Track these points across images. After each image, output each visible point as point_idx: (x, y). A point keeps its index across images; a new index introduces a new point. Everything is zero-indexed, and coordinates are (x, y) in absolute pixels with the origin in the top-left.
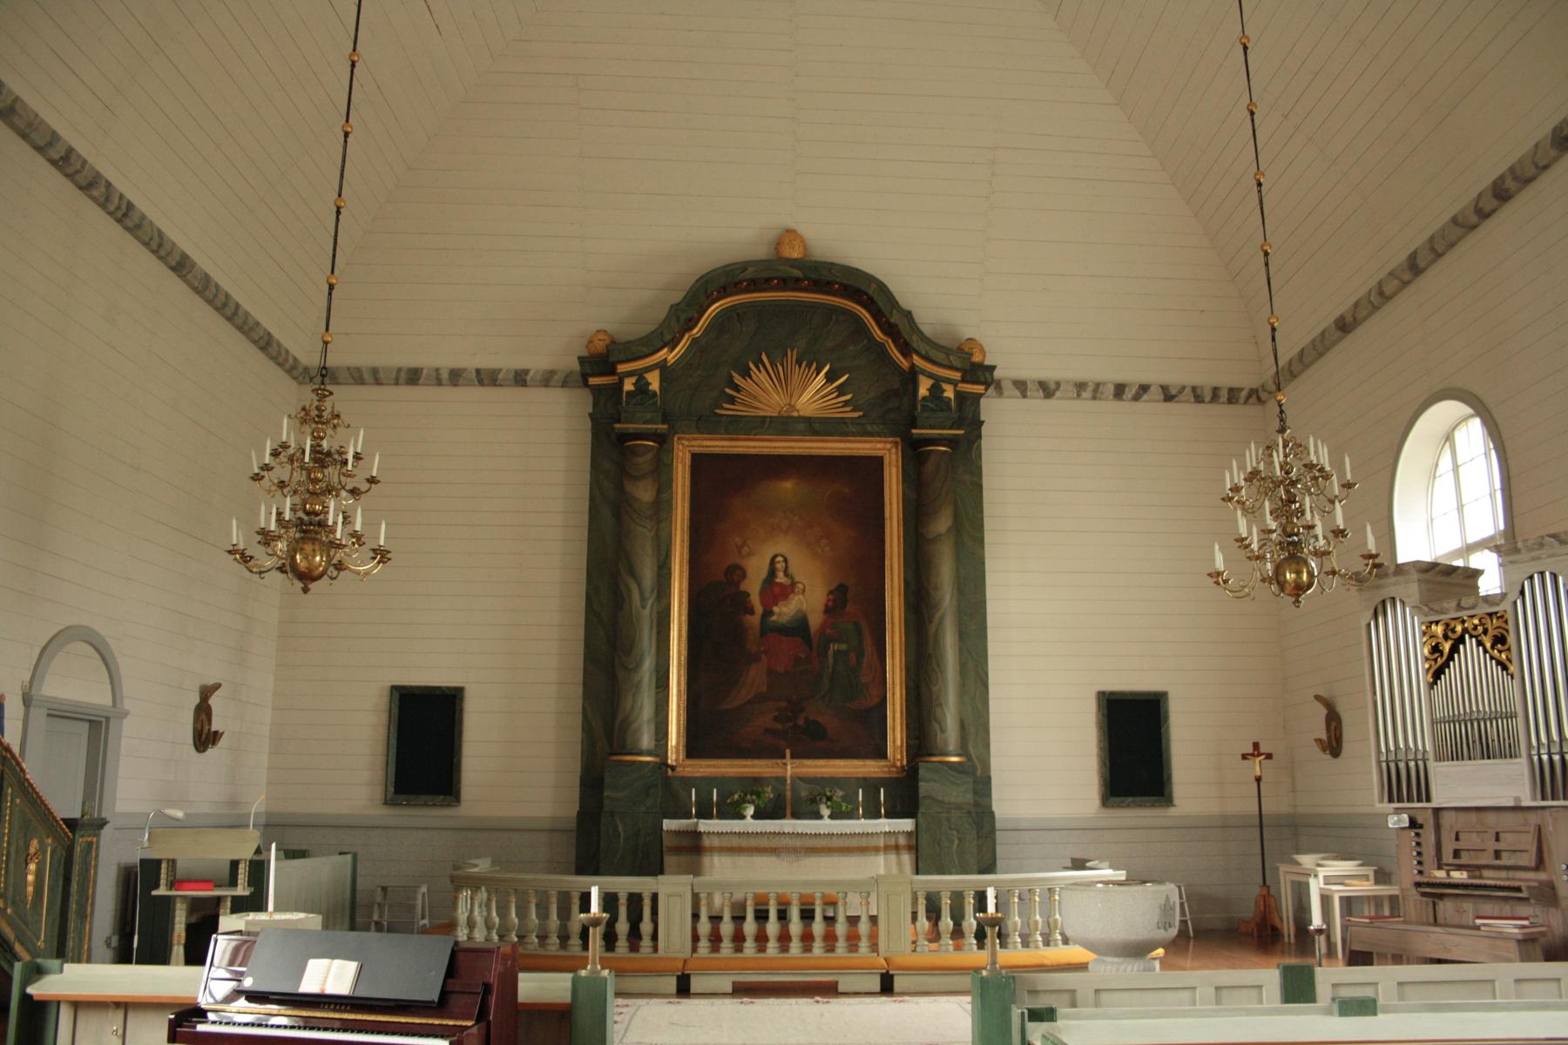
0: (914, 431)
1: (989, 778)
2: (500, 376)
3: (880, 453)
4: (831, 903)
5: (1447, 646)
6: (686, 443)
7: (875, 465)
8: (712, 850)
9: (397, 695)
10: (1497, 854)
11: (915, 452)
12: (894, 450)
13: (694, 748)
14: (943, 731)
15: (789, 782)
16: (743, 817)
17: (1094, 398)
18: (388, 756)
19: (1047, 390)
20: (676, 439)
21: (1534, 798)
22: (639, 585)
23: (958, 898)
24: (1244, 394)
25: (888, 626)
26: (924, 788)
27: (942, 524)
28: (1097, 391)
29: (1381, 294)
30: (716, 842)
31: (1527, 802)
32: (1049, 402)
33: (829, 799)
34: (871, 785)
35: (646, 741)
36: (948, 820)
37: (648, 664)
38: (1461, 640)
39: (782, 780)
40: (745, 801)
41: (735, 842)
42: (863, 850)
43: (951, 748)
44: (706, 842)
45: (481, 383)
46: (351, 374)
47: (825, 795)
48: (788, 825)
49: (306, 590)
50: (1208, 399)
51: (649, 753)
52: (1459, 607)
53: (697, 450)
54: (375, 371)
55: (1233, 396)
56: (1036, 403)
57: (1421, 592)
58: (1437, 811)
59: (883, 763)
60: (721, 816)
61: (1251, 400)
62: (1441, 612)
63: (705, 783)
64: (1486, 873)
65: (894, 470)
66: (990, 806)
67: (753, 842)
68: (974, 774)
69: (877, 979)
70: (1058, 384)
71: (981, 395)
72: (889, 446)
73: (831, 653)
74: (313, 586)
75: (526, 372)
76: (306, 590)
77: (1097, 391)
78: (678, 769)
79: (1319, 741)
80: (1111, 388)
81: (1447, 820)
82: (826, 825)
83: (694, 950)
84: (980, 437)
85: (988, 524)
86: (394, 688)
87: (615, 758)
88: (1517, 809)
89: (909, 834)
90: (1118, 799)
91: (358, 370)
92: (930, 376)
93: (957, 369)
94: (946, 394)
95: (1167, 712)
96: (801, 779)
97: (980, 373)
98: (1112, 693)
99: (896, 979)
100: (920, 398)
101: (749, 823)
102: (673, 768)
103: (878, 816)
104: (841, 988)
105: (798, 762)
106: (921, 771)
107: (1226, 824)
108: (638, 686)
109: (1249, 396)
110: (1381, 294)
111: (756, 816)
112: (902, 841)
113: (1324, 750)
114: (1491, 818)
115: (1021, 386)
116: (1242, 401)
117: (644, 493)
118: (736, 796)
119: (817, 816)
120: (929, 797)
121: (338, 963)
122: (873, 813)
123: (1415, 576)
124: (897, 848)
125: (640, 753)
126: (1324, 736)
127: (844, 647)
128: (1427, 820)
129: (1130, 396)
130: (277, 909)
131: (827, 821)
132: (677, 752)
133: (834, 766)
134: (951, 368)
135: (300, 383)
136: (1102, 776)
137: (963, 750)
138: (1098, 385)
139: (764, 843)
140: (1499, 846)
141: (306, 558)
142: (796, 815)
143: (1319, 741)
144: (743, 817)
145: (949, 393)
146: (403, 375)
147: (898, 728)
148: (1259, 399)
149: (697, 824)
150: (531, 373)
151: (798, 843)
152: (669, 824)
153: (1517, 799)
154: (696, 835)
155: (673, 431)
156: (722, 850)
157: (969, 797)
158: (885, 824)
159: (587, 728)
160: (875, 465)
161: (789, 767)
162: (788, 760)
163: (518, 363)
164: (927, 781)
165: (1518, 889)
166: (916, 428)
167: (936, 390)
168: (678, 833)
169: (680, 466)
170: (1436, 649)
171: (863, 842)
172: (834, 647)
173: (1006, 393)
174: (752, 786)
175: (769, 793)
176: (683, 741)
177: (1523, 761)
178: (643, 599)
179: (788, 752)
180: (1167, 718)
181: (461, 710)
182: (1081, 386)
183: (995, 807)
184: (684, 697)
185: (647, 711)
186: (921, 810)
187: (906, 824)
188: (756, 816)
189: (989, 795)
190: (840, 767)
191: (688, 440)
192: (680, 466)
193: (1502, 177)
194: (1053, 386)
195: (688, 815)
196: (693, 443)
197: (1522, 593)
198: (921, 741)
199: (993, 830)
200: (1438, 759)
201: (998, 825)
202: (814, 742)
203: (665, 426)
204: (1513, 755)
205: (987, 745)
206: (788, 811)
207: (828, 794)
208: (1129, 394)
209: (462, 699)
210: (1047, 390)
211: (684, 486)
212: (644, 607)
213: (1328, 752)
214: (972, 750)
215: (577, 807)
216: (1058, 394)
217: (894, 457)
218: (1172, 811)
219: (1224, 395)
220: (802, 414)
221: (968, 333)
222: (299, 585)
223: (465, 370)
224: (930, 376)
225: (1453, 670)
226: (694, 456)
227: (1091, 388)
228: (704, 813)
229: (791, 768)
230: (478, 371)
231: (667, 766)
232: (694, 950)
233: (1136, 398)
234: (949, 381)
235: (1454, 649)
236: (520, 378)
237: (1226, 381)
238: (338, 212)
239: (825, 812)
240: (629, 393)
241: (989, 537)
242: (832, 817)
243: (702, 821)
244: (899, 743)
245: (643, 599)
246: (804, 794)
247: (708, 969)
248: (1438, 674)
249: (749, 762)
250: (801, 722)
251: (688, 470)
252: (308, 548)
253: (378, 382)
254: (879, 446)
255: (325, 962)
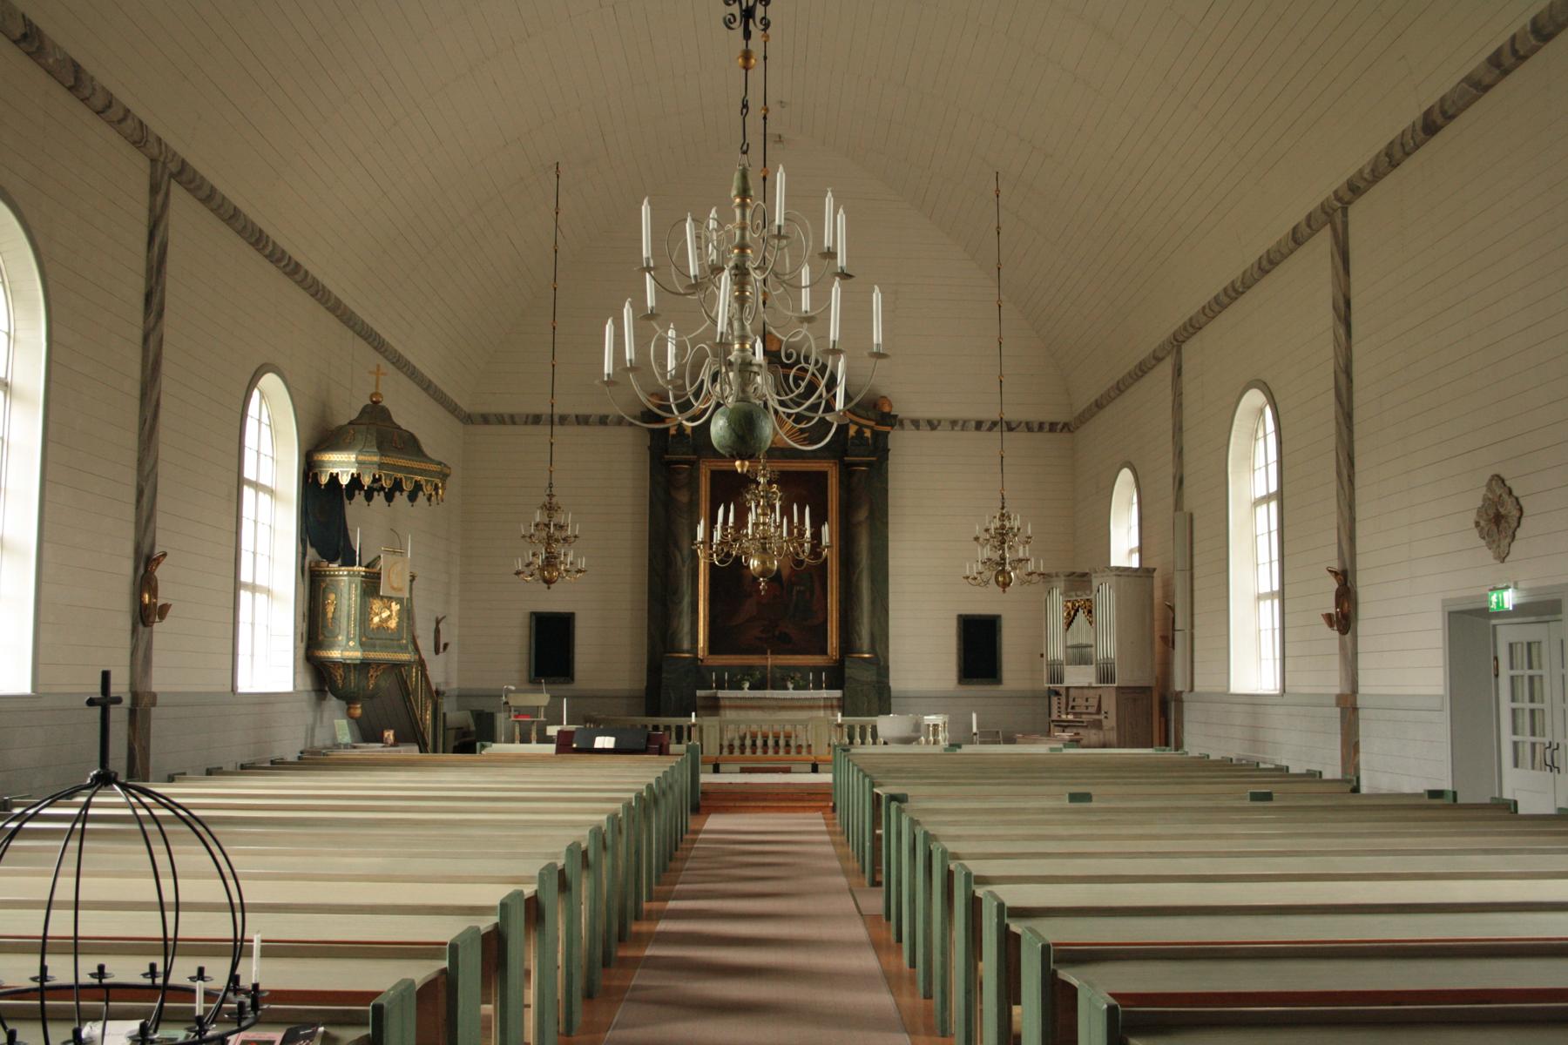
0: (846, 458)
1: (888, 667)
2: (591, 420)
3: (826, 469)
4: (788, 737)
5: (1072, 613)
6: (707, 464)
7: (823, 476)
8: (725, 707)
9: (534, 617)
10: (1087, 707)
11: (847, 471)
12: (834, 468)
13: (713, 648)
14: (860, 639)
15: (769, 668)
16: (743, 689)
17: (962, 430)
18: (530, 654)
19: (933, 425)
20: (701, 462)
21: (1097, 683)
22: (681, 555)
23: (863, 729)
24: (1060, 426)
25: (829, 575)
26: (848, 672)
27: (862, 515)
28: (964, 425)
29: (1515, 52)
30: (727, 703)
31: (1094, 685)
32: (934, 433)
33: (792, 678)
34: (817, 670)
35: (686, 645)
36: (862, 690)
37: (686, 600)
38: (1077, 610)
39: (765, 667)
40: (744, 680)
41: (739, 703)
42: (811, 708)
43: (865, 648)
44: (722, 703)
45: (579, 423)
46: (497, 418)
47: (790, 676)
48: (769, 693)
49: (549, 588)
50: (1036, 430)
51: (688, 652)
52: (1077, 596)
53: (714, 468)
54: (512, 417)
55: (1053, 427)
56: (926, 433)
57: (1065, 586)
58: (1068, 688)
59: (825, 657)
60: (730, 688)
61: (1064, 431)
62: (1071, 596)
63: (721, 669)
64: (1084, 716)
65: (834, 480)
66: (888, 683)
67: (749, 703)
68: (878, 664)
69: (810, 766)
70: (939, 422)
71: (889, 432)
72: (831, 465)
73: (794, 592)
74: (552, 586)
75: (607, 417)
76: (549, 588)
77: (964, 425)
78: (705, 661)
79: (1328, 617)
80: (973, 424)
81: (1072, 692)
82: (791, 693)
83: (721, 753)
84: (887, 459)
85: (891, 511)
86: (533, 614)
87: (668, 655)
88: (1090, 687)
89: (839, 699)
90: (968, 680)
91: (502, 415)
92: (856, 423)
93: (872, 420)
94: (866, 435)
95: (1000, 627)
96: (776, 666)
97: (889, 420)
98: (967, 616)
99: (819, 766)
100: (850, 437)
101: (746, 692)
102: (702, 661)
103: (821, 688)
104: (793, 770)
105: (774, 657)
106: (847, 663)
107: (1034, 695)
108: (681, 613)
109: (1063, 427)
110: (1515, 52)
111: (750, 688)
112: (835, 703)
113: (1331, 626)
114: (1086, 691)
115: (916, 423)
116: (1058, 431)
117: (683, 497)
118: (739, 677)
119: (786, 688)
120: (850, 678)
121: (607, 738)
122: (818, 687)
123: (1063, 578)
124: (832, 707)
125: (683, 652)
126: (1332, 611)
127: (802, 588)
128: (1063, 692)
129: (986, 428)
130: (568, 724)
131: (791, 691)
132: (704, 651)
133: (797, 659)
134: (869, 419)
135: (464, 423)
136: (959, 665)
137: (873, 650)
138: (965, 422)
139: (755, 703)
140: (1087, 704)
141: (549, 573)
142: (774, 688)
143: (1328, 617)
144: (743, 689)
145: (868, 433)
146: (530, 419)
147: (834, 637)
148: (1069, 429)
149: (716, 693)
150: (610, 418)
151: (774, 703)
152: (699, 693)
153: (1090, 683)
154: (716, 699)
155: (699, 459)
156: (731, 707)
157: (874, 678)
158: (824, 693)
159: (651, 637)
160: (823, 476)
161: (769, 660)
162: (769, 656)
163: (603, 411)
164: (849, 668)
165: (1082, 722)
166: (847, 456)
167: (860, 432)
168: (705, 698)
169: (703, 478)
170: (1069, 614)
171: (811, 703)
172: (796, 588)
173: (906, 427)
174: (748, 671)
175: (758, 675)
176: (707, 646)
177: (1094, 666)
178: (683, 562)
179: (769, 651)
180: (1000, 631)
181: (574, 627)
182: (954, 423)
183: (892, 684)
184: (707, 619)
185: (686, 628)
186: (847, 685)
187: (837, 693)
188: (750, 688)
189: (887, 676)
190: (797, 659)
191: (709, 462)
192: (703, 478)
193: (1218, 295)
194: (936, 423)
195: (711, 688)
196: (712, 464)
197: (1098, 591)
198: (848, 643)
199: (889, 697)
200: (1067, 664)
201: (893, 694)
202: (784, 645)
203: (695, 457)
204: (1092, 664)
205: (887, 647)
206: (769, 686)
207: (792, 675)
208: (986, 426)
209: (574, 619)
210: (933, 425)
211: (706, 491)
212: (684, 566)
213: (1335, 628)
214: (878, 649)
215: (645, 684)
216: (939, 428)
217: (834, 472)
218: (1001, 687)
219: (1047, 427)
220: (778, 445)
221: (884, 392)
222: (546, 586)
223: (569, 415)
224: (856, 423)
225: (1074, 624)
226: (713, 473)
227: (960, 423)
228: (720, 686)
229: (771, 660)
230: (577, 416)
231: (698, 659)
232: (721, 753)
233: (990, 429)
234: (867, 427)
235: (1075, 615)
236: (603, 421)
237: (1048, 417)
238: (552, 406)
239: (790, 686)
240: (673, 436)
241: (891, 519)
242: (794, 689)
243: (719, 691)
244: (834, 645)
245: (683, 562)
246: (778, 675)
247: (727, 761)
248: (1069, 624)
249: (746, 657)
250: (777, 633)
251: (708, 480)
252: (550, 569)
253: (514, 423)
254: (826, 465)
255: (603, 738)
